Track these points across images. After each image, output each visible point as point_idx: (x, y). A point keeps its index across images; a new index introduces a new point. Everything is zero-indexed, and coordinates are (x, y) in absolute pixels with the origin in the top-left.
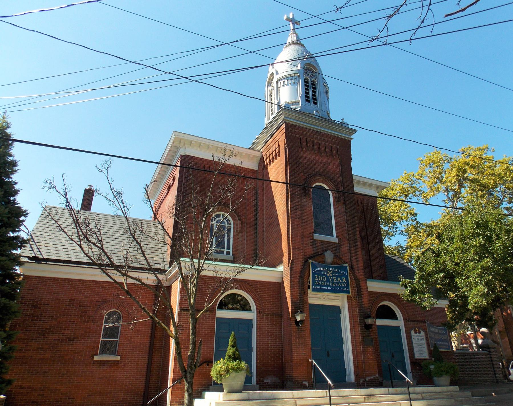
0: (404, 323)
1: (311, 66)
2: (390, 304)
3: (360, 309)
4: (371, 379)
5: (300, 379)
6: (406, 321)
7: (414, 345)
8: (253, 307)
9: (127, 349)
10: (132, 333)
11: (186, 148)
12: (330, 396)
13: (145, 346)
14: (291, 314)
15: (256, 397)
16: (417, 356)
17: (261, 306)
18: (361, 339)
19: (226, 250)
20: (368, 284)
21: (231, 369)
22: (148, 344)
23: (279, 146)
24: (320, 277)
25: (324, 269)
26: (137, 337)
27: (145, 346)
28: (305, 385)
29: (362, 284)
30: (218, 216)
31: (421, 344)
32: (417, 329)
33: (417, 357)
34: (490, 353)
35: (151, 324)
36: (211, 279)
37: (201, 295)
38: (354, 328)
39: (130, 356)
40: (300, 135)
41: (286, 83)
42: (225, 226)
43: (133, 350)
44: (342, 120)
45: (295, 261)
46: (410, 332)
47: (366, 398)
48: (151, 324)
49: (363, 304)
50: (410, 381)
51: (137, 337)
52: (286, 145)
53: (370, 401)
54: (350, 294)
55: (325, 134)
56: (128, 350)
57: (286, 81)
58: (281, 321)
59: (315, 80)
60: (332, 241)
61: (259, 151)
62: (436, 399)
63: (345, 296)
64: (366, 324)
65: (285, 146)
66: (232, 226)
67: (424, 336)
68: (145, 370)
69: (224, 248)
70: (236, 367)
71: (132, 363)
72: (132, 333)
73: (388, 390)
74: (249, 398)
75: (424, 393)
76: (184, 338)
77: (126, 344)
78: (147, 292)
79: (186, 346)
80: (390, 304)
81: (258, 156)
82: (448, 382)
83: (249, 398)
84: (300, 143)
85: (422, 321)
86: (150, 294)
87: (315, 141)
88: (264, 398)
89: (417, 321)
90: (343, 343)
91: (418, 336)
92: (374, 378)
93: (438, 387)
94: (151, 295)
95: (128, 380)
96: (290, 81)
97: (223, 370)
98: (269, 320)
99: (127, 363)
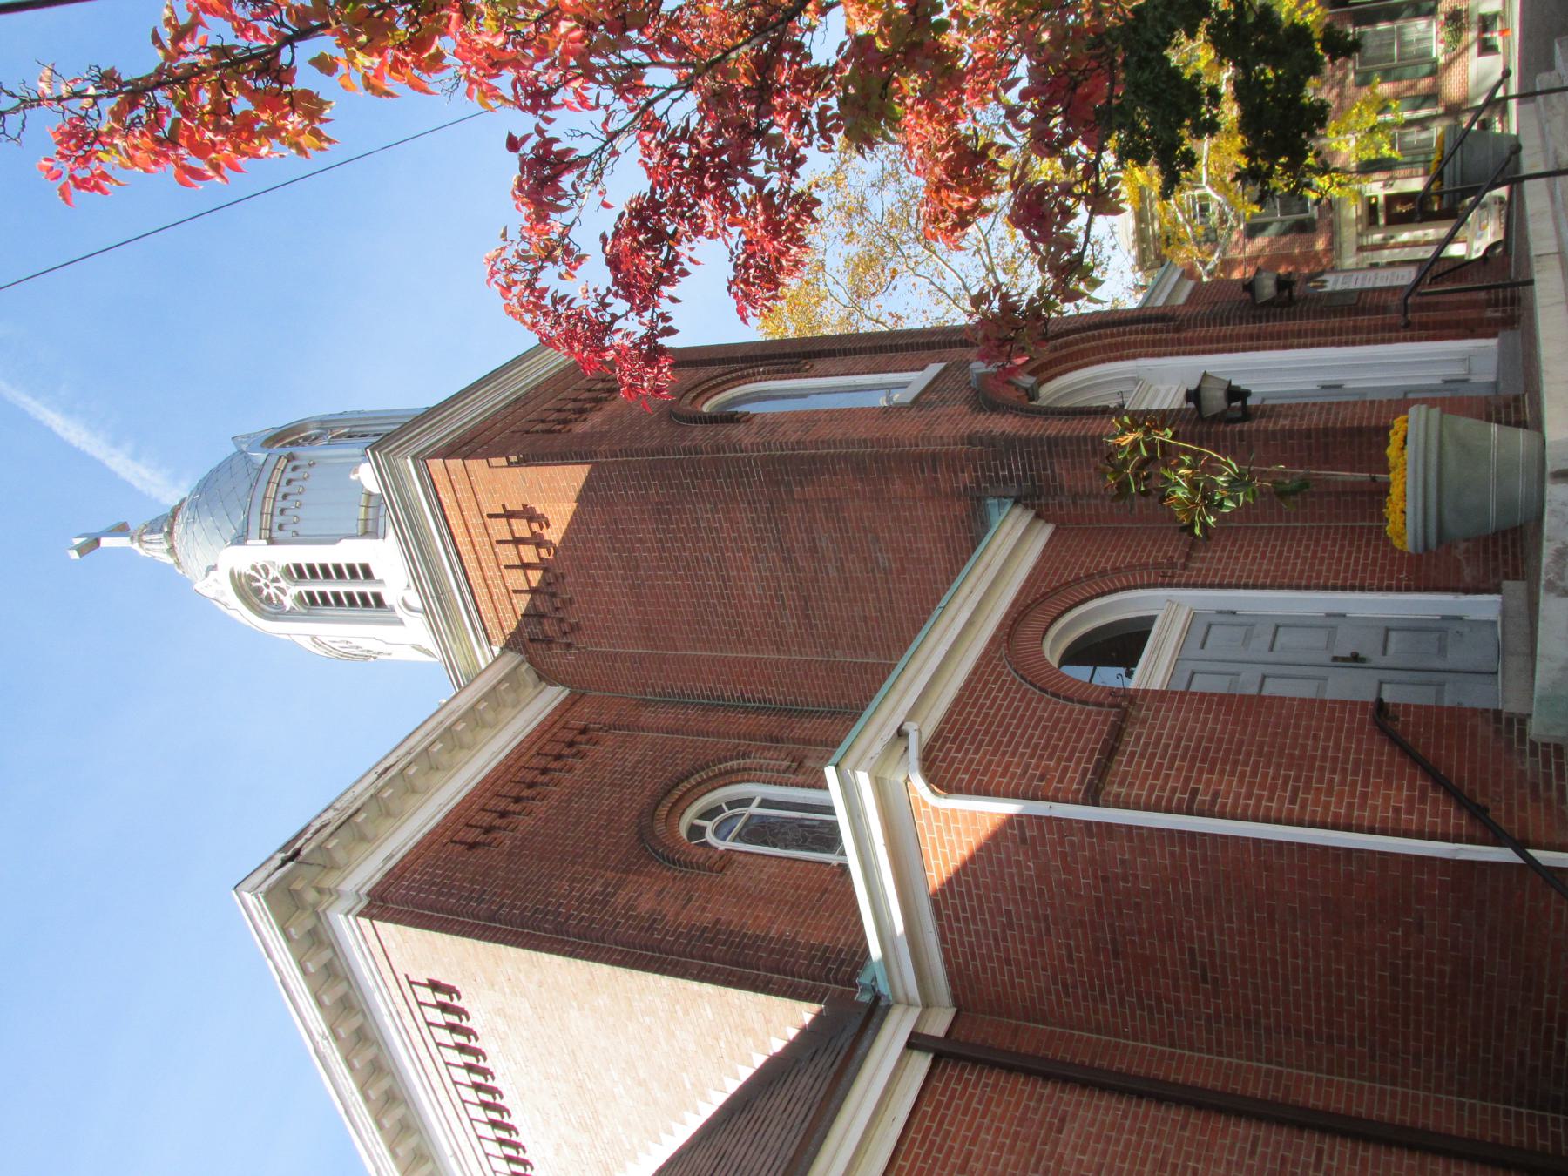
22: (1243, 1130)
23: (509, 515)
27: (1254, 1145)
42: (751, 817)
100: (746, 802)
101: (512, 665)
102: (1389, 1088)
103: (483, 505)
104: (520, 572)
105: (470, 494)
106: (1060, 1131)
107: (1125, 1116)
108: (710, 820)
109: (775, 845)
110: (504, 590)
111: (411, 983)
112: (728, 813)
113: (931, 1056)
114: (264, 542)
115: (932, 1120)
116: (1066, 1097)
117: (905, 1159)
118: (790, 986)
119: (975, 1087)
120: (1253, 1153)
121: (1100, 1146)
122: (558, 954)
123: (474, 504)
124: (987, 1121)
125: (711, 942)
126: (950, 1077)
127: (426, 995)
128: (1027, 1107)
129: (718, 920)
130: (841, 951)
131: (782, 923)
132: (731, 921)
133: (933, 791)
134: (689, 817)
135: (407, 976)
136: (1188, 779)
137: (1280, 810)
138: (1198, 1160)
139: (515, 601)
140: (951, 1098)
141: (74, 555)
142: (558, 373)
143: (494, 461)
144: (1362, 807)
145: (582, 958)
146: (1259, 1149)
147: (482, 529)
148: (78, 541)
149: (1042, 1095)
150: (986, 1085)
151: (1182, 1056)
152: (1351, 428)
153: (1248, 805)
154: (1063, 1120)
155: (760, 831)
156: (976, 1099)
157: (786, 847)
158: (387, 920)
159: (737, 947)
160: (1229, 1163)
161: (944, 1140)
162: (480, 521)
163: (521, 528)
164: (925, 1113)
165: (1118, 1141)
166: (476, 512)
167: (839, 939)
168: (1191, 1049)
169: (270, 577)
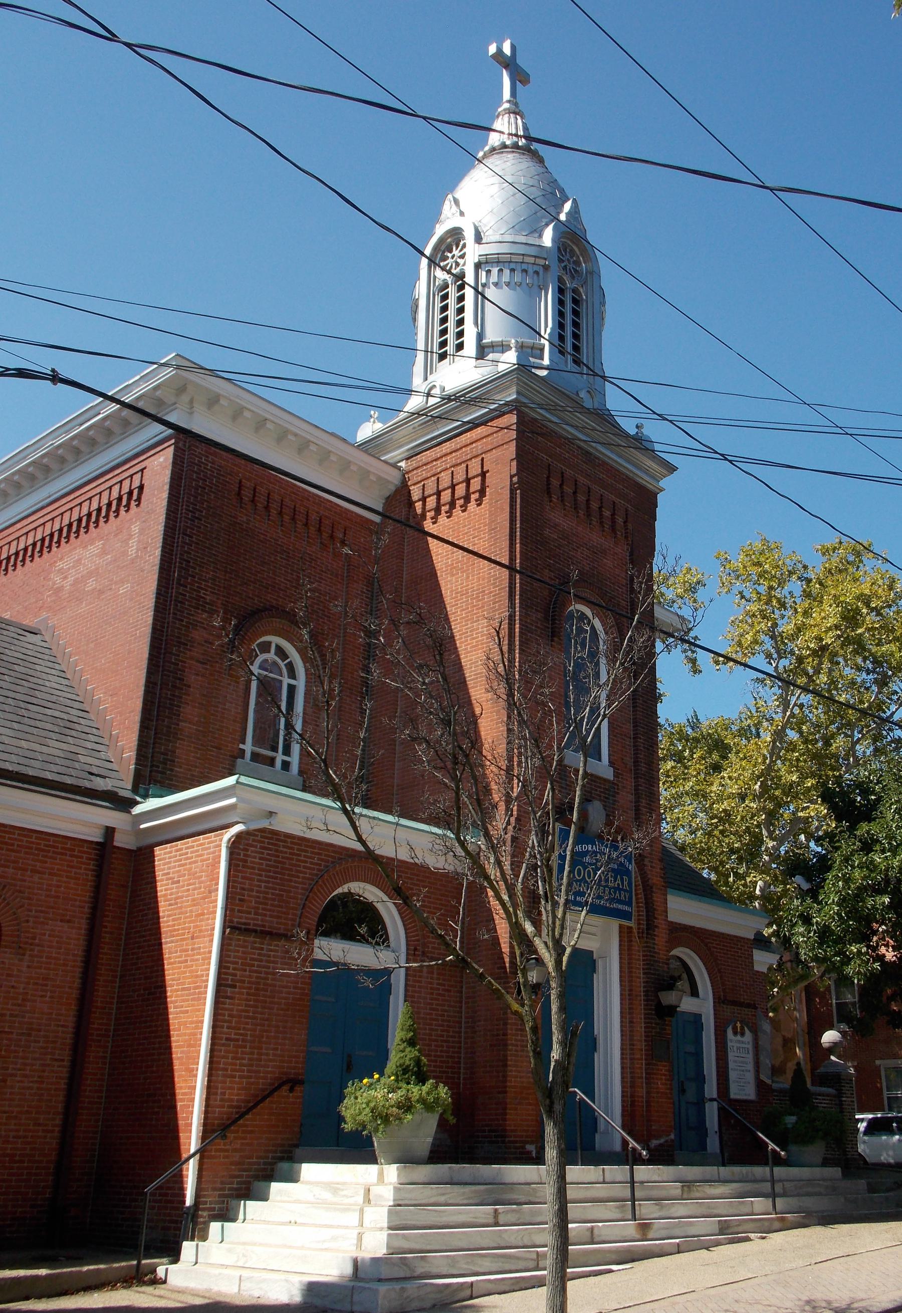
0: (714, 1006)
1: (577, 246)
2: (689, 956)
3: (648, 964)
4: (661, 1145)
5: (521, 1136)
6: (720, 1001)
7: (731, 1065)
8: (398, 934)
9: (12, 1033)
10: (28, 983)
11: (191, 413)
12: (632, 1182)
13: (63, 1026)
14: (507, 965)
15: (466, 1177)
16: (735, 1093)
17: (417, 935)
18: (645, 1041)
19: (280, 757)
20: (670, 905)
21: (418, 1101)
22: (70, 1020)
23: (483, 474)
24: (579, 869)
25: (590, 849)
26: (42, 996)
27: (63, 1026)
28: (530, 1152)
29: (657, 897)
30: (265, 647)
31: (742, 1062)
32: (739, 1025)
33: (735, 1094)
34: (840, 1094)
35: (82, 961)
36: (306, 846)
37: (281, 890)
38: (630, 1013)
39: (21, 1054)
40: (550, 456)
41: (494, 277)
42: (281, 681)
43: (29, 1035)
44: (637, 427)
45: (523, 819)
46: (725, 1031)
47: (685, 1188)
48: (82, 961)
49: (655, 953)
50: (778, 1149)
51: (42, 996)
52: (515, 479)
53: (693, 1195)
54: (632, 924)
55: (604, 463)
56: (14, 1036)
57: (495, 271)
58: (462, 982)
59: (581, 290)
60: (601, 775)
61: (395, 466)
62: (808, 1194)
63: (614, 925)
64: (659, 1002)
65: (511, 481)
66: (301, 684)
67: (751, 1043)
68: (61, 1098)
69: (275, 749)
70: (431, 1099)
71: (26, 1076)
72: (28, 983)
73: (772, 1171)
74: (452, 1178)
75: (787, 1181)
76: (237, 1010)
77: (11, 1015)
78: (73, 861)
79: (241, 1034)
80: (689, 956)
81: (388, 482)
82: (819, 1160)
83: (452, 1178)
84: (548, 477)
85: (749, 1006)
86: (80, 868)
87: (582, 479)
88: (483, 1181)
89: (741, 1004)
90: (595, 1048)
91: (739, 1042)
92: (666, 1141)
93: (806, 1169)
94: (82, 871)
95: (12, 1127)
96: (507, 272)
97: (393, 1102)
98: (435, 976)
99: (12, 1075)
100: (292, 674)
101: (389, 479)
102: (104, 1095)
103: (489, 454)
104: (449, 484)
105: (496, 444)
106: (61, 921)
107: (74, 955)
108: (276, 654)
109: (256, 704)
110: (439, 470)
111: (142, 470)
112: (282, 664)
113: (101, 840)
114: (476, 260)
115: (62, 848)
116: (84, 921)
117: (36, 838)
118: (147, 742)
119: (85, 869)
120: (58, 1026)
121: (55, 944)
122: (158, 585)
123: (490, 447)
124: (65, 879)
125: (172, 686)
126: (90, 854)
127: (136, 483)
128: (76, 900)
129: (189, 686)
130: (172, 770)
131: (190, 728)
132: (189, 695)
133: (230, 839)
134: (275, 640)
135: (145, 468)
136: (243, 982)
137: (221, 1033)
138: (51, 997)
139: (433, 479)
140: (76, 857)
141: (492, 49)
142: (623, 474)
143: (514, 463)
144: (224, 1076)
145: (156, 602)
146: (60, 1029)
147: (475, 453)
148: (507, 49)
149: (83, 907)
150: (87, 875)
151: (115, 982)
152: (507, 1060)
153: (224, 1015)
154: (69, 921)
155: (268, 689)
156: (78, 871)
157: (255, 711)
158: (175, 455)
159: (170, 704)
160: (51, 1014)
161: (51, 858)
162: (480, 452)
163: (476, 484)
164: (67, 844)
165: (59, 953)
166: (485, 449)
167: (181, 767)
168: (120, 987)
169: (459, 260)
